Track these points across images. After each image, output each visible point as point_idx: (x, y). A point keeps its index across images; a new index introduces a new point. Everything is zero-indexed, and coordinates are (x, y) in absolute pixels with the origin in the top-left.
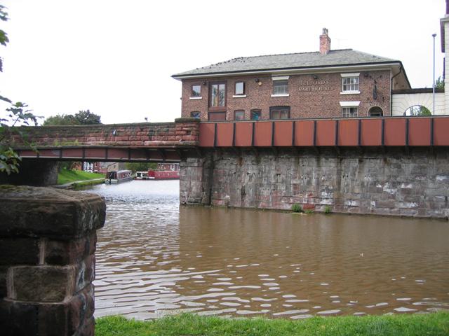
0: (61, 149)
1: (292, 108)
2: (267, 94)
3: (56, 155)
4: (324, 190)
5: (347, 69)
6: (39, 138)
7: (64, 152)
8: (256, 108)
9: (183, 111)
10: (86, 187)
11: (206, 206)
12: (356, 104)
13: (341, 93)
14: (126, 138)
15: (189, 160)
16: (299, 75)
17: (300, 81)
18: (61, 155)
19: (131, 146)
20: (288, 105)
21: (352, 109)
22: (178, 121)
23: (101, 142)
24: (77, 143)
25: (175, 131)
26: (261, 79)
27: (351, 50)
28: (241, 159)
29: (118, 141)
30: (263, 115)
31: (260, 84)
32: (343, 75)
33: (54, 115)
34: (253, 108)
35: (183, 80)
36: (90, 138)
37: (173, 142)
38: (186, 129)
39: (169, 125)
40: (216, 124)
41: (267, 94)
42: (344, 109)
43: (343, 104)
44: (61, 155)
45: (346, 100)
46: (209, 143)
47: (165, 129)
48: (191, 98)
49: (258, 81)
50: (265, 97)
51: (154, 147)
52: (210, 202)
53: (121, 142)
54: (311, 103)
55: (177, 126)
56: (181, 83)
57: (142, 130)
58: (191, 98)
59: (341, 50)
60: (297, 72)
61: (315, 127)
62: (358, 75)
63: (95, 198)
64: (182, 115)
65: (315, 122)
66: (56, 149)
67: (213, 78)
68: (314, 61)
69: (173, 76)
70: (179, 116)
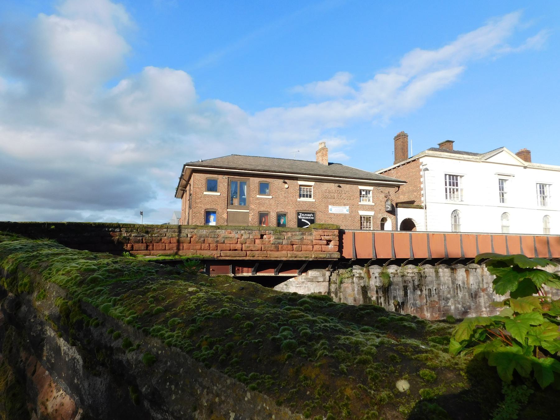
8: (283, 210)
20: (314, 210)
34: (278, 210)
45: (364, 210)
61: (445, 240)
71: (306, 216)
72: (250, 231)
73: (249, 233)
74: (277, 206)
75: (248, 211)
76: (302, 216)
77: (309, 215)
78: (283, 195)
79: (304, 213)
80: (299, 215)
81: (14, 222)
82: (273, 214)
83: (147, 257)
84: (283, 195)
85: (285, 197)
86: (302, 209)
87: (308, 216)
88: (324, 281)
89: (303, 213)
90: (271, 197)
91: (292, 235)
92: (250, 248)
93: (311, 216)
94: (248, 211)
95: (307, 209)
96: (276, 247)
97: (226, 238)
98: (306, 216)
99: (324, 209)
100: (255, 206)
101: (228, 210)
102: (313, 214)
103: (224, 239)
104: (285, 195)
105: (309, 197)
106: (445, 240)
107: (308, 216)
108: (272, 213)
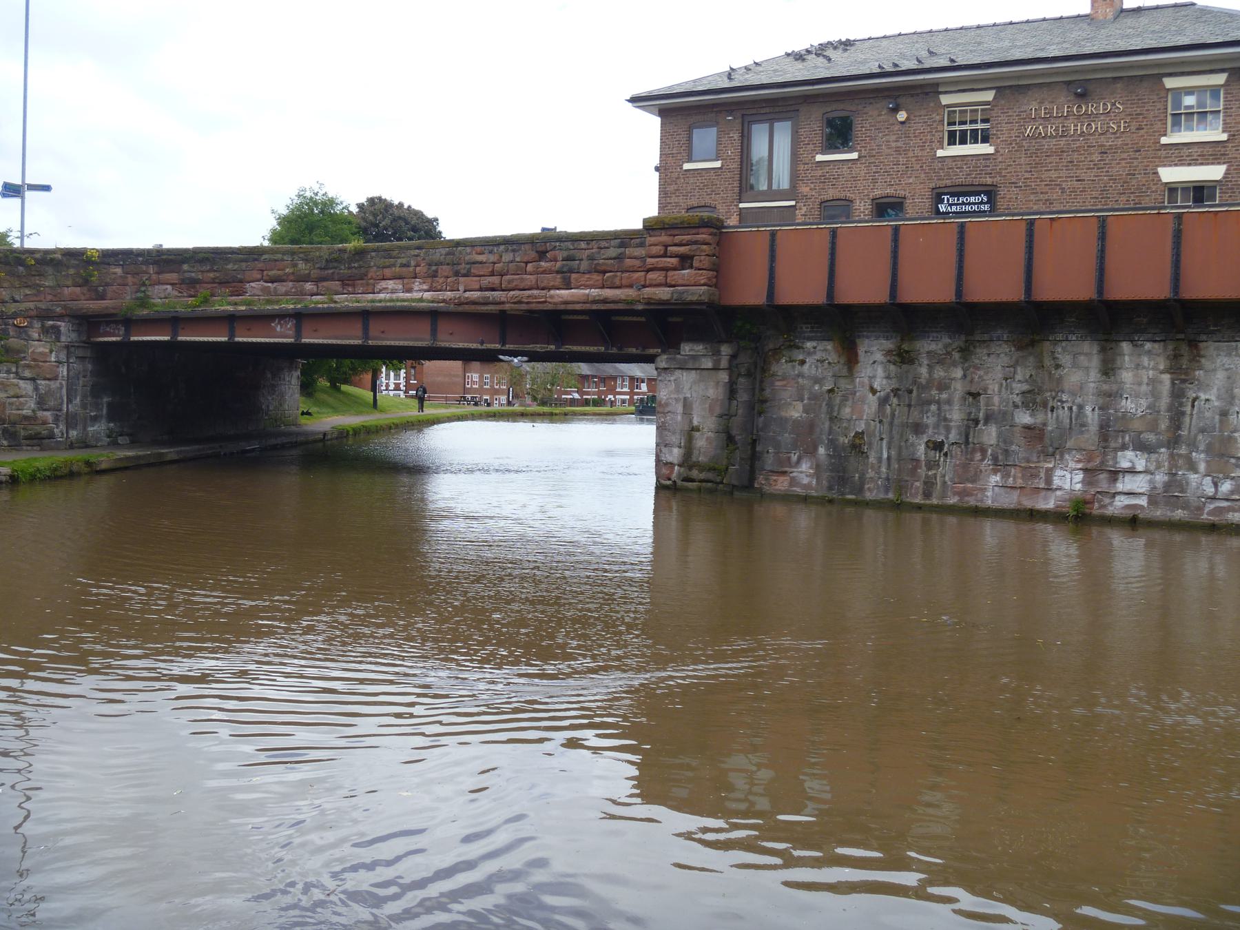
0: (299, 317)
1: (1002, 192)
2: (922, 148)
3: (282, 335)
4: (1124, 447)
5: (1183, 62)
6: (235, 285)
7: (307, 327)
8: (889, 191)
9: (664, 193)
10: (557, 417)
11: (737, 494)
12: (1214, 172)
13: (1164, 140)
14: (495, 280)
15: (687, 349)
16: (1028, 87)
17: (1031, 105)
18: (298, 333)
19: (507, 307)
20: (989, 181)
21: (1200, 192)
22: (651, 226)
23: (420, 294)
24: (345, 301)
25: (643, 259)
26: (901, 101)
27: (1193, 4)
28: (1086, 337)
29: (468, 292)
30: (910, 210)
31: (902, 116)
32: (1170, 83)
33: (416, 207)
34: (878, 193)
35: (664, 113)
36: (383, 284)
37: (488, 294)
38: (682, 249)
39: (624, 238)
40: (773, 234)
41: (922, 148)
42: (1172, 189)
43: (1170, 174)
44: (298, 333)
45: (1181, 162)
46: (750, 293)
47: (613, 252)
48: (819, 158)
49: (896, 110)
50: (918, 159)
51: (578, 307)
52: (752, 479)
53: (475, 295)
54: (1064, 173)
55: (653, 240)
56: (657, 121)
57: (542, 255)
58: (819, 158)
59: (1157, 8)
60: (1021, 76)
61: (1103, 237)
62: (1220, 79)
63: (285, 440)
64: (662, 206)
65: (1103, 222)
66: (282, 316)
67: (754, 102)
68: (1076, 43)
69: (634, 100)
70: (653, 211)
71: (963, 203)
72: (515, 247)
73: (513, 251)
74: (875, 181)
75: (793, 203)
76: (951, 205)
77: (972, 199)
78: (893, 145)
79: (958, 195)
80: (942, 201)
81: (194, 248)
82: (862, 204)
83: (234, 297)
84: (893, 145)
85: (898, 150)
86: (948, 182)
87: (969, 204)
88: (716, 369)
89: (952, 195)
90: (854, 156)
91: (601, 248)
92: (514, 284)
93: (982, 203)
94: (793, 203)
95: (969, 180)
96: (564, 279)
97: (474, 263)
98: (963, 203)
99: (1027, 175)
100: (812, 186)
101: (742, 205)
102: (988, 193)
103: (468, 266)
104: (899, 144)
105: (960, 144)
106: (1103, 237)
107: (969, 204)
108: (858, 202)
